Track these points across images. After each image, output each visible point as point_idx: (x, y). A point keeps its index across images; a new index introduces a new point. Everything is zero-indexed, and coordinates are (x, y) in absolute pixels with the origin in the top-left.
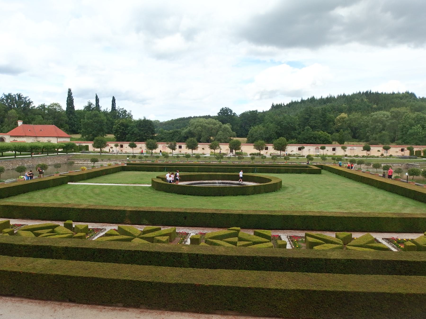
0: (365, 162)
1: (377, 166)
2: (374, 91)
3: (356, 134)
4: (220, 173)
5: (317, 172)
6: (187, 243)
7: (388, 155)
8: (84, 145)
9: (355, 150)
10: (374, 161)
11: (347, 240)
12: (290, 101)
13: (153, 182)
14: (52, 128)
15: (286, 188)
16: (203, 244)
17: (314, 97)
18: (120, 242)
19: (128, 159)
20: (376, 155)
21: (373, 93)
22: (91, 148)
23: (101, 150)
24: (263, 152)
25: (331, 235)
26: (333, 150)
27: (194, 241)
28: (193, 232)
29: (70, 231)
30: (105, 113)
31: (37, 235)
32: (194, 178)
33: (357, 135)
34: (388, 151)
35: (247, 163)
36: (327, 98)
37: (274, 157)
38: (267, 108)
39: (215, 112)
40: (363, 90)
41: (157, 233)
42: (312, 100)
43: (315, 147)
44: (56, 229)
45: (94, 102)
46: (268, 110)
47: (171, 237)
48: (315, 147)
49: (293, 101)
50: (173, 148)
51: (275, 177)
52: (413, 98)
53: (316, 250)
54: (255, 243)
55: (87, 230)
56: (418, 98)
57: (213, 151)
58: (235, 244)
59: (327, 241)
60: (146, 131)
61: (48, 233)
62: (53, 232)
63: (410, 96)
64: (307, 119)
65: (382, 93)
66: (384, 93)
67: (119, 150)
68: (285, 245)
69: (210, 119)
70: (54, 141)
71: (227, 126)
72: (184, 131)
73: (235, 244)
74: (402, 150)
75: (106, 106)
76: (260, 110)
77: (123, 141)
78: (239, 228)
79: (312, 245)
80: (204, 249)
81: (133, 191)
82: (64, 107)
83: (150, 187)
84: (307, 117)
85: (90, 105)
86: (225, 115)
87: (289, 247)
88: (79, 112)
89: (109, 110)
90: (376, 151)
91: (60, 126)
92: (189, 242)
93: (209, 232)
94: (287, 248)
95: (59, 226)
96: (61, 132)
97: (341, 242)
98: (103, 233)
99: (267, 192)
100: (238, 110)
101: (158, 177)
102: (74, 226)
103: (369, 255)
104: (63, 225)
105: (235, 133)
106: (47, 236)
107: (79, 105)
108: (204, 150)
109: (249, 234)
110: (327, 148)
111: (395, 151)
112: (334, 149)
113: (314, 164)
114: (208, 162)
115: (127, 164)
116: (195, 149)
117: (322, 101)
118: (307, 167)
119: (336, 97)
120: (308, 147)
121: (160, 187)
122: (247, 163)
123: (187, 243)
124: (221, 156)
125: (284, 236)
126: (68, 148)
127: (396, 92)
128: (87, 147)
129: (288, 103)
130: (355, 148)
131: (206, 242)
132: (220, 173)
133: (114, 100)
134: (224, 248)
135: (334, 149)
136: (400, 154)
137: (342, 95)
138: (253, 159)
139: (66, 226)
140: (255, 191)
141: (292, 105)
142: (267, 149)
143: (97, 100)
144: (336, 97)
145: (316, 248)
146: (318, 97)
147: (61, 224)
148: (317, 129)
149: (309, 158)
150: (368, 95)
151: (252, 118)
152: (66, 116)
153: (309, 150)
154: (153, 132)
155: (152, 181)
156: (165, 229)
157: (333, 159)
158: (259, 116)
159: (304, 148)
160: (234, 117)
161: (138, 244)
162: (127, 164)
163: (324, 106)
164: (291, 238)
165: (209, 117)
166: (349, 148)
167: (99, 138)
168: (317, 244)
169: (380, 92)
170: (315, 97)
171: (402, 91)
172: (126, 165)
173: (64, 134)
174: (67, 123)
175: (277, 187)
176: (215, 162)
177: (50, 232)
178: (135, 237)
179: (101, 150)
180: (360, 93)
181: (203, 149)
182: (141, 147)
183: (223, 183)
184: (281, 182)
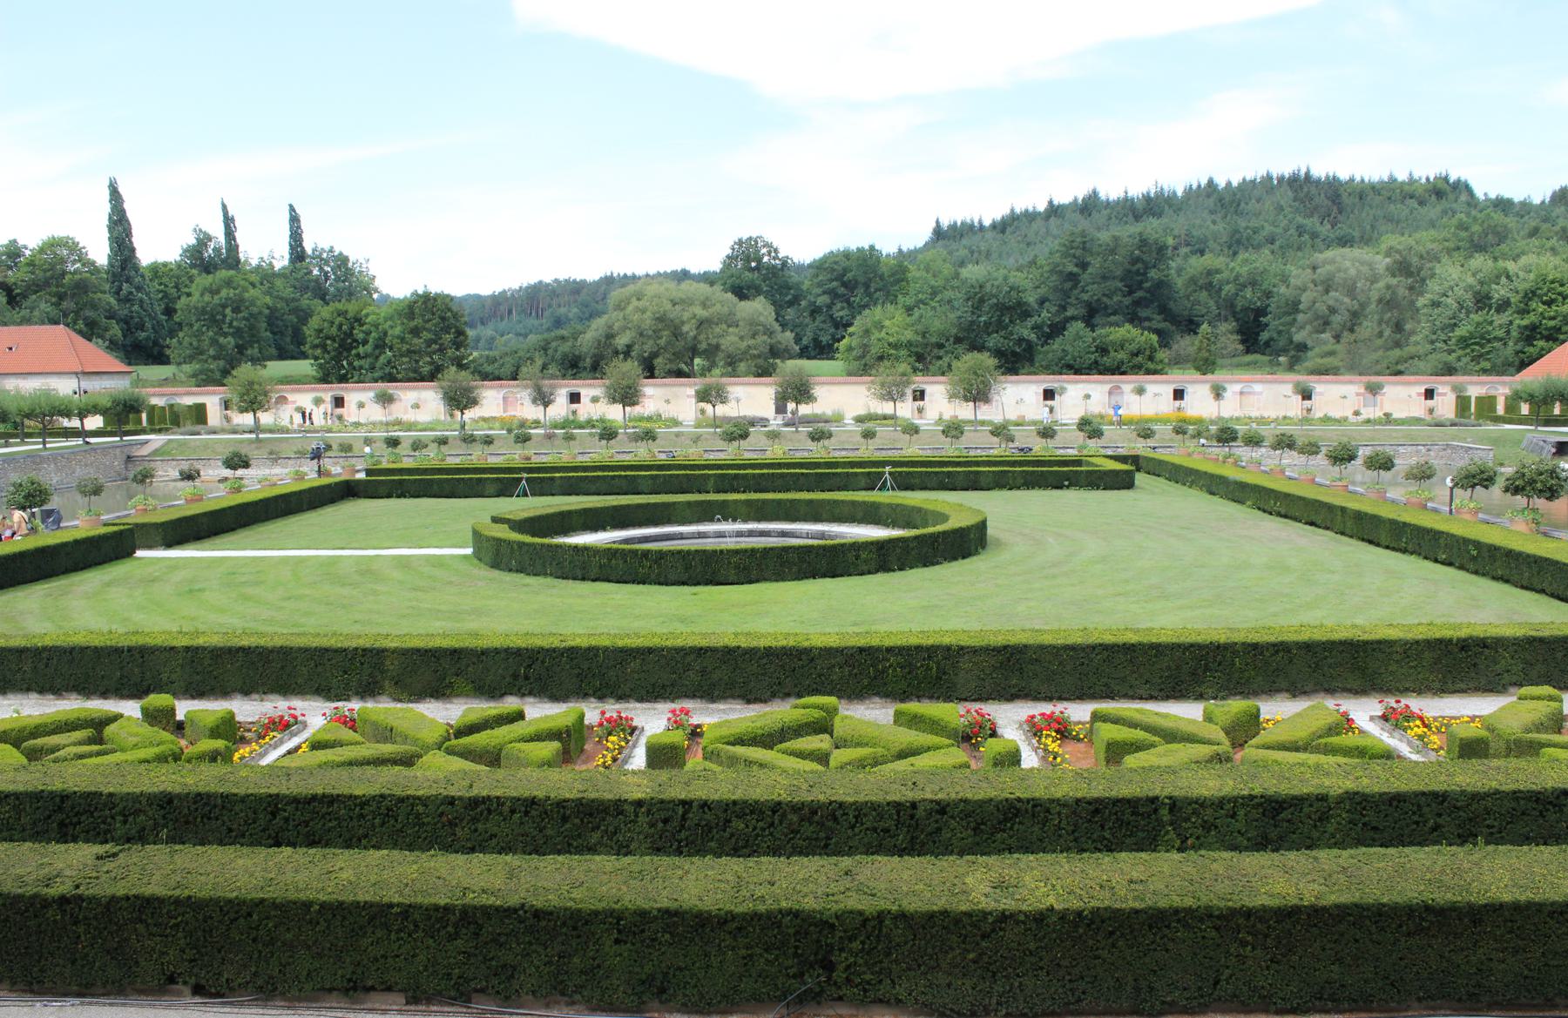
0: (1300, 443)
1: (1343, 456)
2: (1319, 171)
3: (1260, 335)
4: (742, 497)
5: (1121, 481)
6: (631, 766)
7: (1379, 414)
8: (189, 401)
9: (1260, 397)
10: (1330, 438)
11: (1245, 729)
12: (1006, 211)
13: (478, 538)
14: (59, 339)
15: (937, 222)
16: (695, 762)
17: (1094, 192)
18: (370, 771)
19: (367, 450)
20: (1336, 414)
21: (1318, 182)
22: (214, 415)
23: (256, 420)
24: (906, 409)
25: (1187, 712)
26: (1175, 398)
27: (661, 756)
28: (653, 721)
29: (166, 736)
30: (266, 275)
31: (33, 755)
32: (560, 518)
33: (1264, 336)
34: (1379, 398)
35: (844, 453)
36: (1147, 198)
37: (953, 429)
38: (916, 236)
39: (709, 258)
40: (1283, 167)
41: (517, 729)
42: (1090, 205)
43: (1107, 387)
44: (109, 730)
45: (218, 232)
46: (920, 244)
47: (571, 741)
48: (1107, 387)
49: (1018, 211)
50: (544, 399)
51: (957, 508)
52: (1463, 198)
53: (1131, 770)
54: (902, 755)
55: (228, 729)
56: (1481, 197)
57: (708, 408)
58: (822, 758)
59: (1172, 736)
60: (434, 340)
61: (80, 743)
62: (99, 740)
63: (1446, 191)
64: (1072, 277)
65: (1352, 180)
66: (1358, 179)
67: (311, 416)
68: (1014, 758)
69: (687, 286)
70: (65, 387)
71: (759, 308)
72: (573, 333)
73: (822, 758)
74: (1429, 394)
75: (263, 245)
76: (888, 247)
77: (343, 379)
78: (832, 700)
79: (1116, 752)
80: (703, 780)
81: (416, 575)
82: (99, 252)
83: (465, 557)
84: (1071, 268)
85: (204, 239)
86: (753, 273)
87: (1029, 760)
88: (157, 270)
89: (282, 260)
90: (1338, 398)
91: (90, 331)
92: (639, 759)
93: (713, 717)
94: (1024, 765)
95: (116, 718)
96: (96, 354)
97: (1222, 736)
98: (294, 739)
99: (927, 561)
100: (802, 244)
101: (495, 520)
102: (180, 716)
103: (1333, 777)
104: (138, 714)
105: (789, 335)
106: (81, 757)
107: (158, 245)
108: (671, 403)
109: (872, 716)
110: (1151, 389)
111: (1402, 398)
112: (1179, 394)
113: (1103, 452)
114: (693, 453)
115: (369, 472)
116: (633, 404)
117: (1132, 210)
118: (1078, 463)
119: (1180, 193)
120: (1080, 386)
121: (528, 553)
122: (844, 453)
123: (631, 766)
124: (739, 430)
125: (1010, 720)
126: (123, 414)
127: (1402, 176)
128: (199, 414)
129: (999, 218)
130: (1258, 387)
131: (710, 756)
132: (742, 497)
133: (295, 219)
134: (782, 776)
135: (1179, 394)
136: (1418, 408)
137: (1204, 182)
138: (868, 435)
139: (152, 716)
140: (883, 558)
141: (1010, 225)
142: (920, 395)
143: (229, 222)
144: (1180, 193)
145: (1131, 761)
146: (1111, 191)
147: (131, 709)
148: (1113, 318)
149: (1090, 428)
150: (1300, 185)
151: (856, 281)
152: (107, 287)
153: (1088, 397)
154: (460, 340)
155: (476, 534)
156: (540, 712)
157: (1180, 431)
158: (884, 270)
159: (1063, 390)
160: (787, 273)
161: (441, 773)
162: (369, 472)
163: (1134, 229)
164: (1034, 729)
165: (684, 275)
166: (1237, 387)
167: (245, 371)
168: (1136, 747)
169: (1343, 176)
170: (1102, 196)
171: (1426, 170)
172: (361, 476)
173: (113, 363)
174: (111, 316)
175: (966, 543)
176: (729, 453)
177: (90, 741)
178: (427, 748)
179: (256, 420)
180: (1269, 177)
181: (668, 401)
182: (421, 405)
183: (751, 533)
184: (982, 526)
